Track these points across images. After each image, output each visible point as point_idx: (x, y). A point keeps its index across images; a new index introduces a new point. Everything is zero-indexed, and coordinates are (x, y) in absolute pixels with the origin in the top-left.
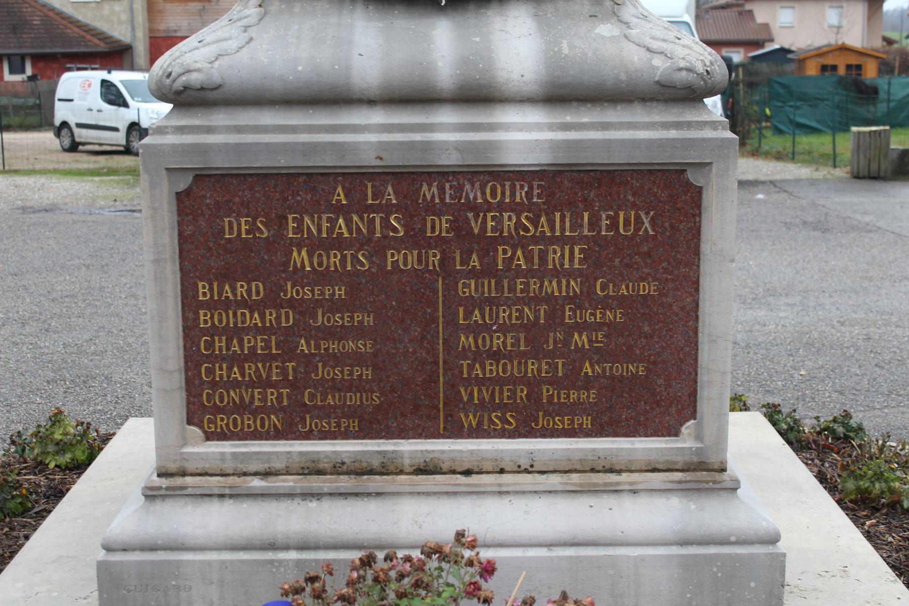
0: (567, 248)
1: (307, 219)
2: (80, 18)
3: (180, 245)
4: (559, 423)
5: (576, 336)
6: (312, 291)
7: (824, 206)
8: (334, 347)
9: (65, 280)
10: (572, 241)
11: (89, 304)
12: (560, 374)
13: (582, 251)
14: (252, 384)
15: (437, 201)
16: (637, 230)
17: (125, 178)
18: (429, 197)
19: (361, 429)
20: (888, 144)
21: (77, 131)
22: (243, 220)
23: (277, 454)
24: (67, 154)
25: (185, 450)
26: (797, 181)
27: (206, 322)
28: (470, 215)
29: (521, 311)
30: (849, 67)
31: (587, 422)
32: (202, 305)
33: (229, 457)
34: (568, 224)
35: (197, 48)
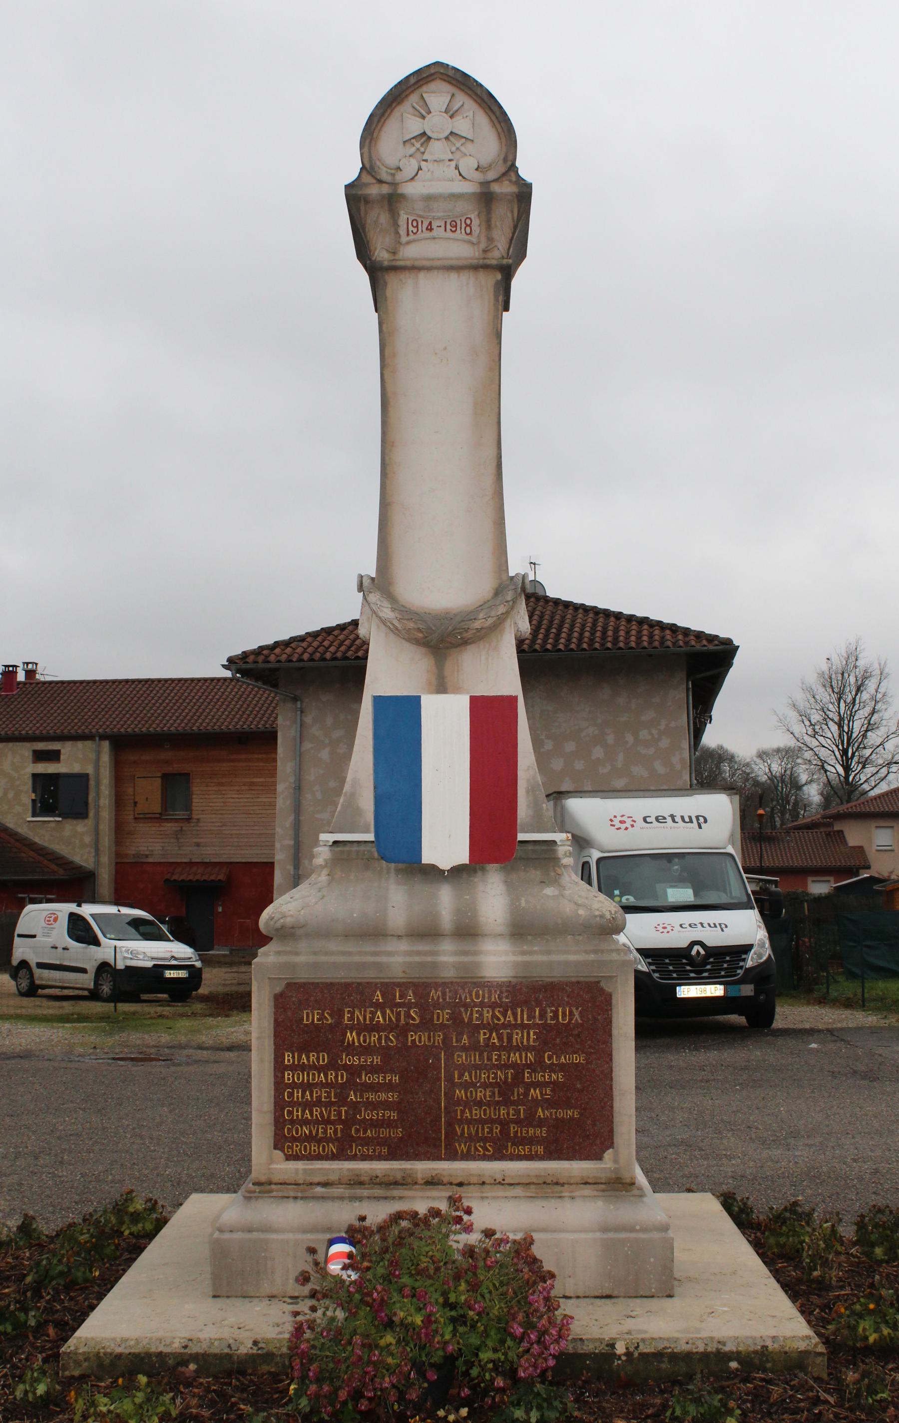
0: (525, 1031)
1: (357, 1012)
4: (522, 1150)
5: (532, 1090)
6: (359, 1059)
7: (880, 1055)
8: (372, 1096)
9: (65, 1121)
10: (528, 1027)
11: (96, 1142)
12: (522, 1116)
13: (535, 1033)
14: (317, 1122)
15: (441, 1000)
16: (570, 1020)
17: (99, 1025)
18: (435, 998)
19: (389, 1154)
21: (37, 972)
22: (316, 1012)
23: (333, 1170)
24: (26, 1001)
25: (271, 1166)
26: (858, 1029)
28: (462, 1010)
29: (496, 1074)
31: (540, 1150)
32: (287, 1068)
33: (301, 1172)
34: (525, 1016)
35: (290, 902)
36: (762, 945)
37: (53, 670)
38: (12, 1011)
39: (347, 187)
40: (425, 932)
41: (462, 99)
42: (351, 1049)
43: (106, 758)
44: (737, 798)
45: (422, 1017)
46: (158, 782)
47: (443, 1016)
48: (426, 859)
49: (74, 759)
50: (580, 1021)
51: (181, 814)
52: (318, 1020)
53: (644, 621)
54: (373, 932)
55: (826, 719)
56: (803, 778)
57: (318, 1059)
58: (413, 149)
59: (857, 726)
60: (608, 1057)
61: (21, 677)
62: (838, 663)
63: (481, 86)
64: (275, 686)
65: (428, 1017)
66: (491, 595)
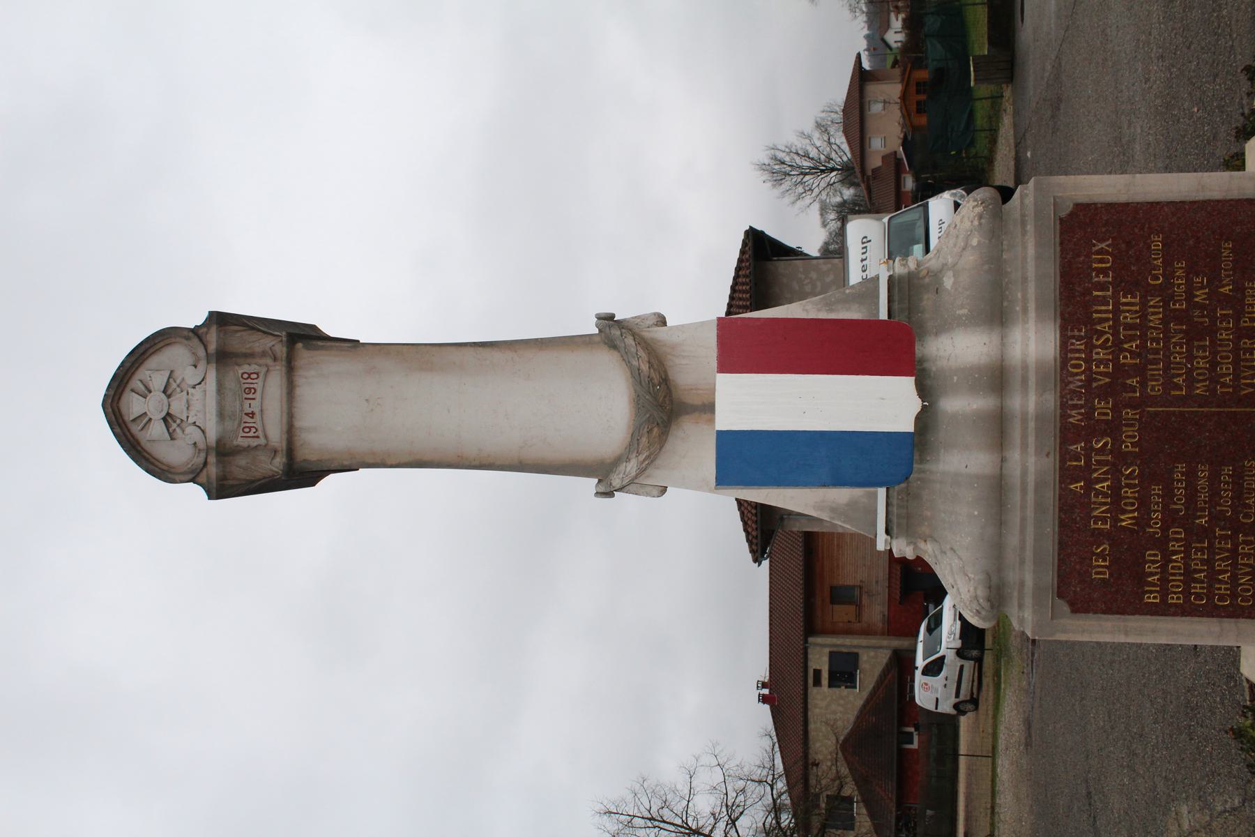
1: (1096, 513)
2: (871, 686)
3: (1113, 613)
6: (1155, 511)
10: (1117, 304)
14: (1235, 565)
16: (1107, 253)
20: (984, 56)
21: (962, 698)
22: (1095, 563)
24: (982, 707)
26: (1015, 126)
27: (1178, 598)
28: (1094, 385)
29: (1175, 344)
30: (918, 92)
36: (955, 195)
37: (763, 672)
38: (990, 721)
39: (210, 498)
40: (998, 428)
41: (135, 383)
42: (1143, 522)
43: (819, 640)
44: (850, 217)
45: (1104, 434)
46: (836, 607)
47: (1103, 408)
48: (909, 427)
49: (820, 660)
50: (1110, 242)
51: (857, 592)
52: (1104, 560)
53: (733, 289)
54: (997, 491)
55: (801, 183)
56: (838, 199)
57: (1154, 562)
58: (178, 430)
59: (806, 164)
60: (1154, 207)
61: (766, 691)
62: (766, 176)
63: (123, 362)
64: (773, 532)
65: (1103, 426)
66: (616, 354)
